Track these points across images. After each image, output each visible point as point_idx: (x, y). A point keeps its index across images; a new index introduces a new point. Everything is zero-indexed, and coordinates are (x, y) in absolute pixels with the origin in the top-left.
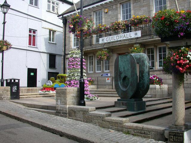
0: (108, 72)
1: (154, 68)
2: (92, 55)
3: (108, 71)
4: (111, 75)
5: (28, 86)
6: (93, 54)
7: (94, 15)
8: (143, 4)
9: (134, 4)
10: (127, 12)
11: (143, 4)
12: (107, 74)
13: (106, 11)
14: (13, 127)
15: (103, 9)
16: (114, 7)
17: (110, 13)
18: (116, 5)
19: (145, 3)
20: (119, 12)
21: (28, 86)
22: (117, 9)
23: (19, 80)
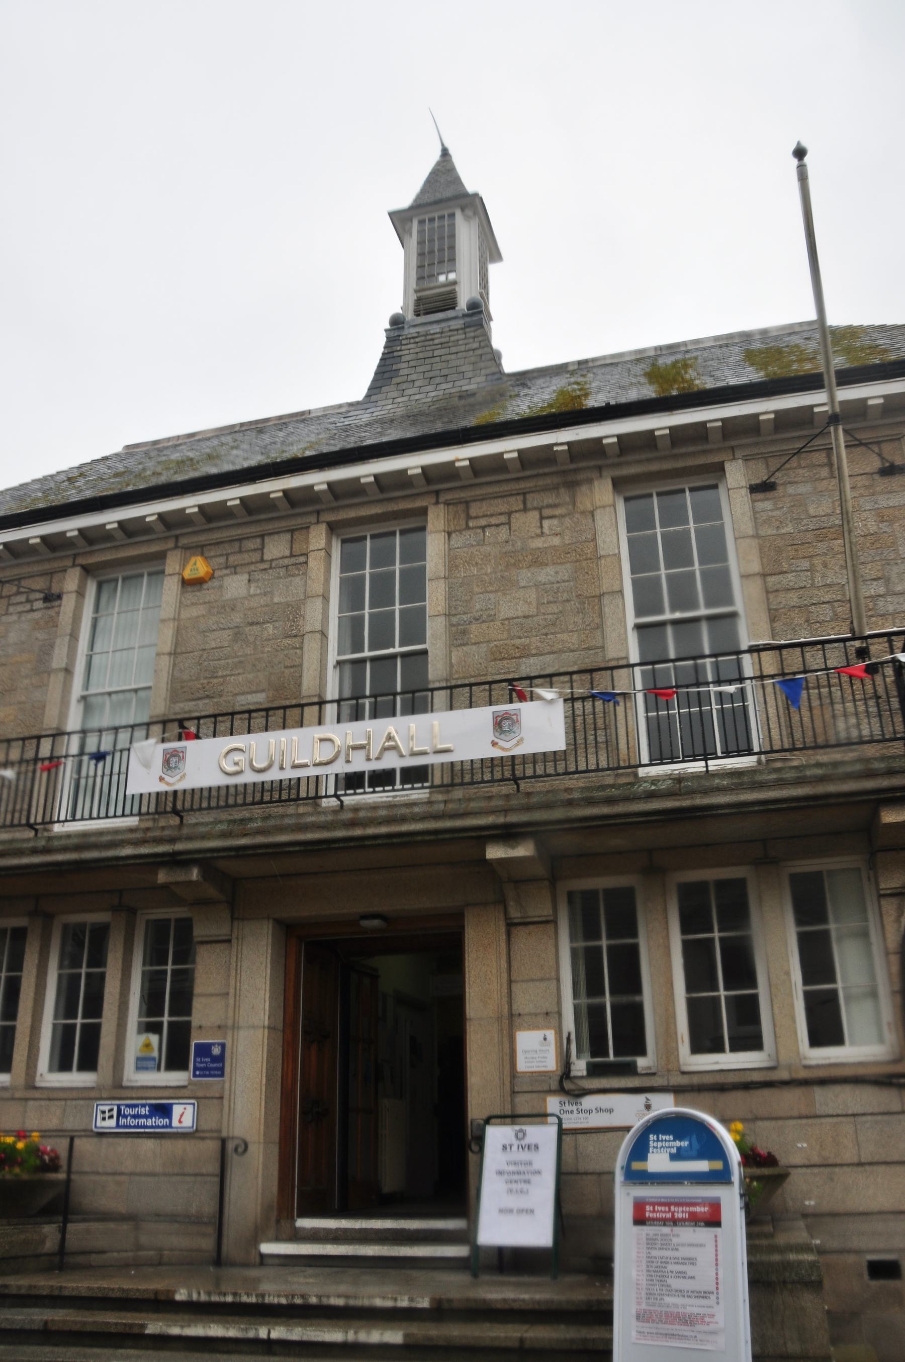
0: (178, 1092)
1: (642, 1062)
2: (20, 922)
3: (177, 1078)
4: (209, 1124)
5: (171, 1105)
6: (115, 909)
7: (81, 594)
8: (538, 543)
9: (457, 540)
10: (382, 595)
11: (538, 543)
12: (164, 1111)
13: (198, 567)
14: (685, 1323)
15: (178, 552)
16: (277, 548)
17: (235, 586)
18: (292, 531)
19: (556, 541)
20: (316, 587)
21: (171, 1105)
22: (297, 562)
23: (223, 1046)
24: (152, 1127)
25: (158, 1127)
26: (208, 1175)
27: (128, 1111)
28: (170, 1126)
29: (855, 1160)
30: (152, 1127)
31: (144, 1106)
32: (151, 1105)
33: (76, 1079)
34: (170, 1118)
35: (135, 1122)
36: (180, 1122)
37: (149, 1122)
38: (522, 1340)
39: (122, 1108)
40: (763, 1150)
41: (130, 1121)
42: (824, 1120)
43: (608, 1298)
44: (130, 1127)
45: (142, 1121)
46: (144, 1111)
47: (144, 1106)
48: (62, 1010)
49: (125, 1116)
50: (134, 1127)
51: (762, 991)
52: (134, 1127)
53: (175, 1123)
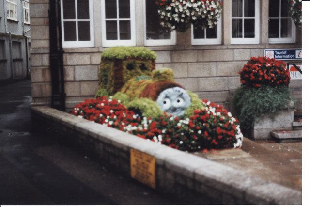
24: (288, 58)
25: (290, 58)
26: (39, 18)
27: (278, 53)
28: (295, 58)
29: (218, 63)
30: (288, 58)
31: (284, 51)
32: (287, 51)
33: (244, 40)
34: (295, 55)
35: (281, 57)
36: (299, 56)
37: (287, 57)
38: (273, 119)
39: (276, 52)
40: (148, 140)
41: (279, 56)
42: (212, 92)
43: (300, 137)
44: (279, 58)
45: (284, 56)
46: (284, 53)
47: (284, 51)
48: (288, 22)
49: (277, 55)
50: (281, 58)
51: (91, 20)
52: (281, 58)
53: (297, 57)
